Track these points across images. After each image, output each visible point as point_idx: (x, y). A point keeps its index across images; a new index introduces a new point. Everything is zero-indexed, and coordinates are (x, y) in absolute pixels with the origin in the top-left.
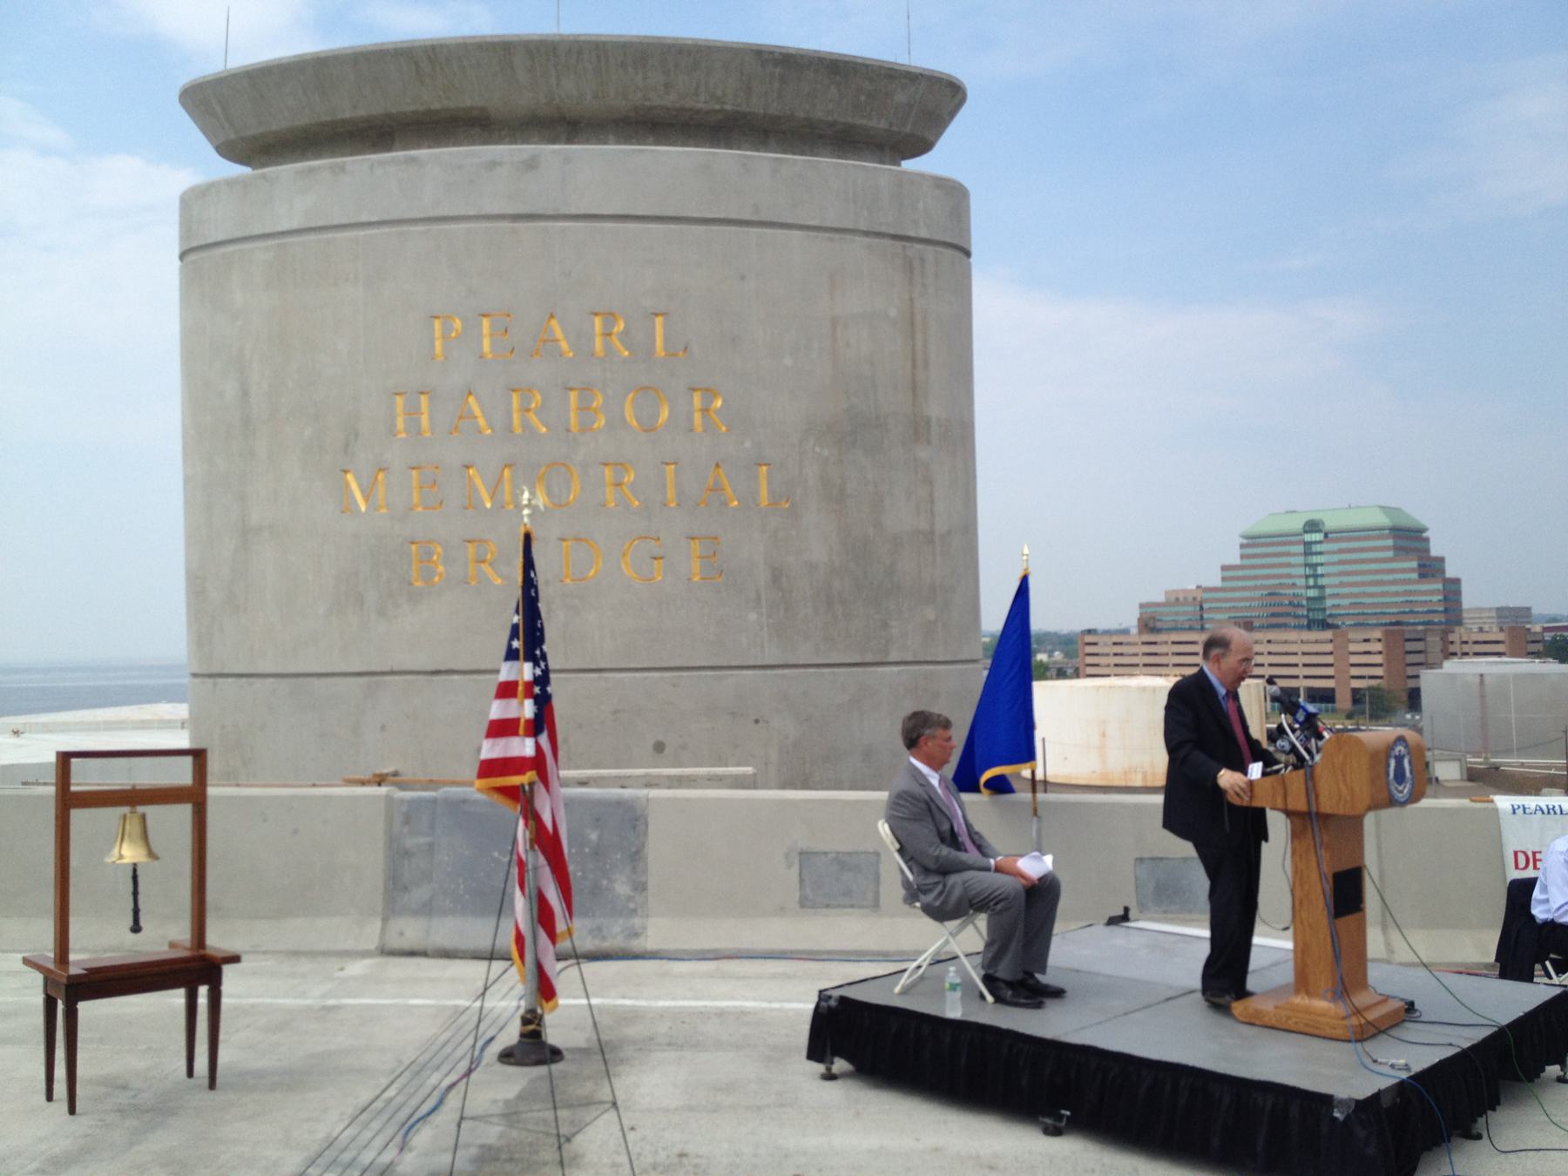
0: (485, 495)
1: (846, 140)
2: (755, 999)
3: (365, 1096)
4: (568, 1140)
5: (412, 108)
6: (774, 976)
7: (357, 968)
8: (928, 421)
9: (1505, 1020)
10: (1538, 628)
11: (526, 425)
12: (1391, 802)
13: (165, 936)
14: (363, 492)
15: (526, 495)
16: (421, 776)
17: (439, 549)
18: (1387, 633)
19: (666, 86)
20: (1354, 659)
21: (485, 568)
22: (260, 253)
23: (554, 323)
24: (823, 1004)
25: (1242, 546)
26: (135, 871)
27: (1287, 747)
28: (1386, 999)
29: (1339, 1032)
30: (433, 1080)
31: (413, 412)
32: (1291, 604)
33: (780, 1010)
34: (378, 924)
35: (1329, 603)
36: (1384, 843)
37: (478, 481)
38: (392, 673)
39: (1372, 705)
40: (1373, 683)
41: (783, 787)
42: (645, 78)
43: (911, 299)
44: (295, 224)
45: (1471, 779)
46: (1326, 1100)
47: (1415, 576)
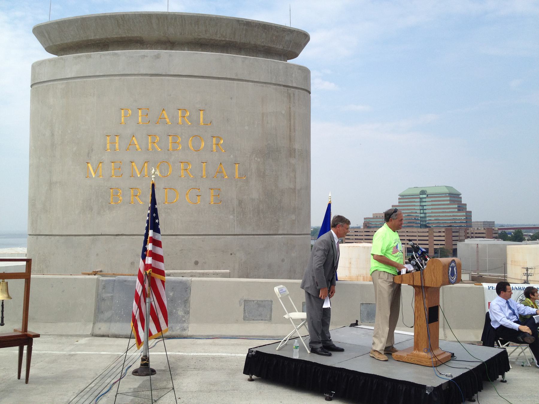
0: (138, 172)
1: (268, 52)
2: (226, 352)
3: (83, 386)
4: (156, 401)
5: (116, 36)
6: (233, 345)
7: (83, 341)
8: (295, 150)
9: (485, 360)
10: (497, 229)
11: (153, 148)
12: (450, 283)
13: (11, 327)
14: (94, 170)
15: (153, 171)
16: (110, 272)
17: (121, 191)
18: (446, 230)
19: (206, 31)
20: (435, 238)
21: (137, 198)
22: (60, 85)
23: (164, 112)
24: (250, 354)
25: (399, 199)
26: (3, 303)
27: (415, 263)
28: (444, 352)
29: (428, 364)
30: (108, 381)
31: (113, 143)
32: (415, 219)
33: (234, 356)
34: (91, 325)
35: (428, 219)
36: (449, 297)
37: (135, 167)
38: (101, 235)
39: (441, 253)
40: (442, 246)
41: (240, 277)
42: (198, 28)
43: (290, 108)
44: (73, 76)
45: (473, 280)
46: (424, 387)
47: (456, 210)
